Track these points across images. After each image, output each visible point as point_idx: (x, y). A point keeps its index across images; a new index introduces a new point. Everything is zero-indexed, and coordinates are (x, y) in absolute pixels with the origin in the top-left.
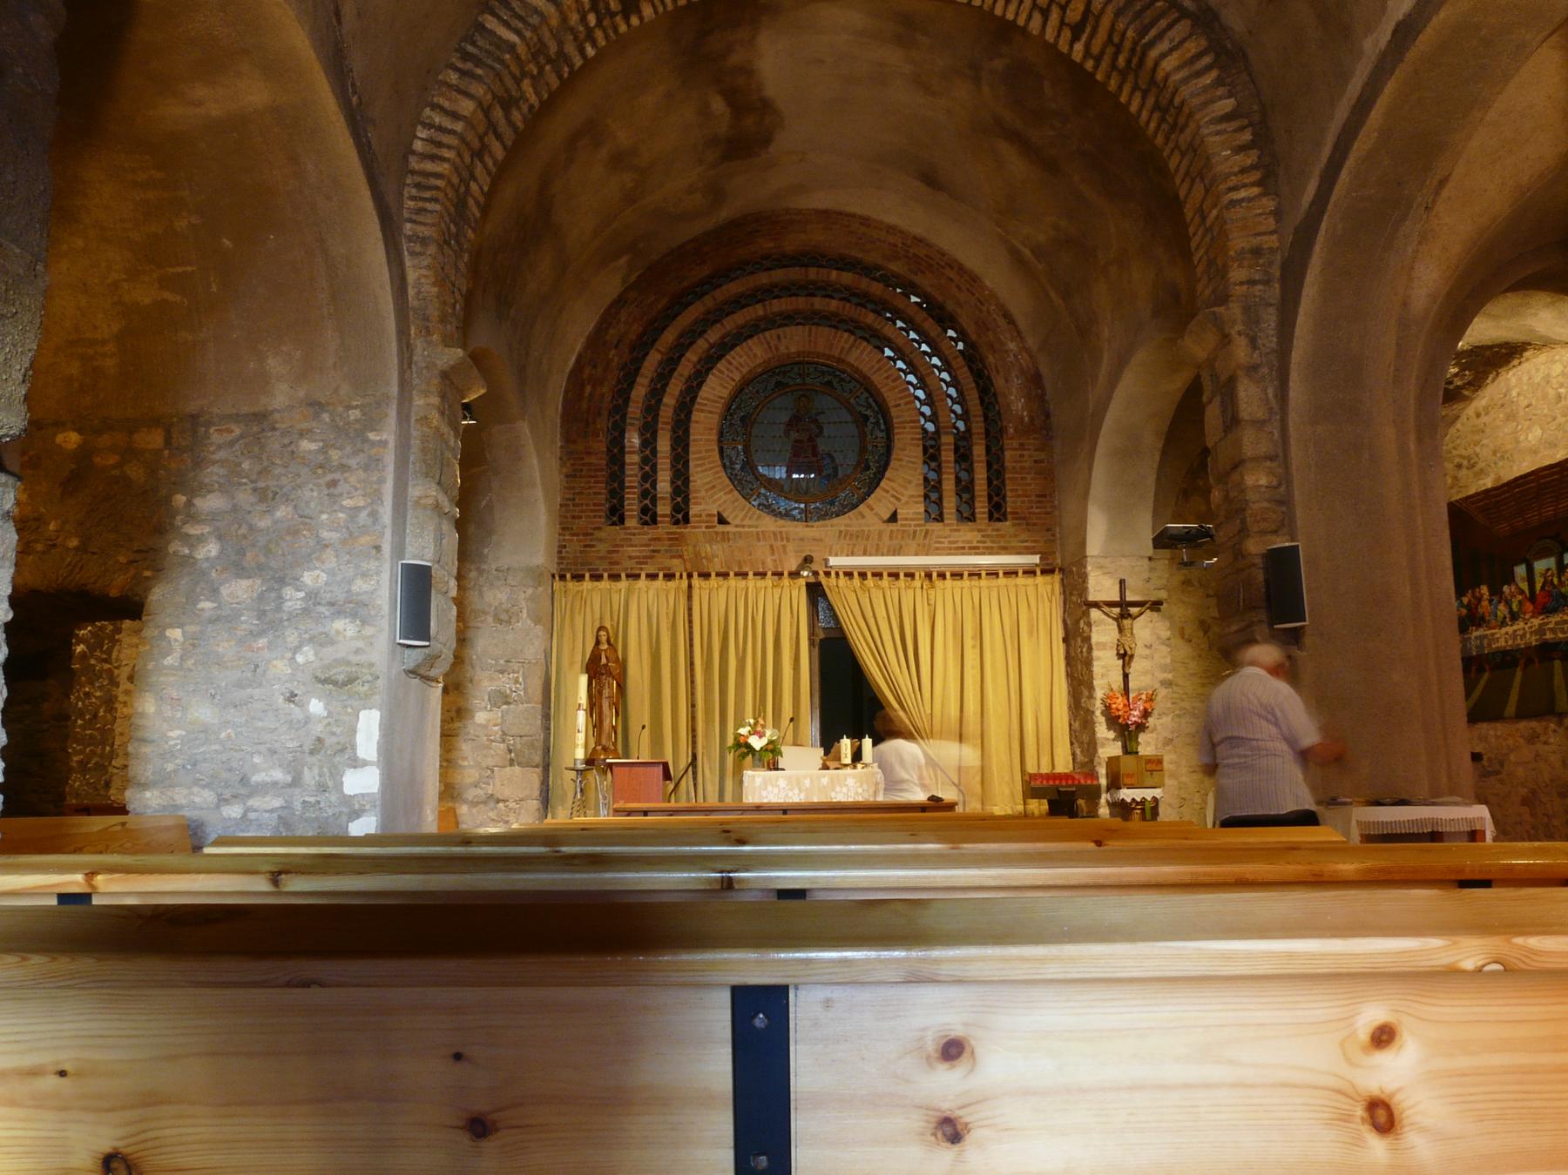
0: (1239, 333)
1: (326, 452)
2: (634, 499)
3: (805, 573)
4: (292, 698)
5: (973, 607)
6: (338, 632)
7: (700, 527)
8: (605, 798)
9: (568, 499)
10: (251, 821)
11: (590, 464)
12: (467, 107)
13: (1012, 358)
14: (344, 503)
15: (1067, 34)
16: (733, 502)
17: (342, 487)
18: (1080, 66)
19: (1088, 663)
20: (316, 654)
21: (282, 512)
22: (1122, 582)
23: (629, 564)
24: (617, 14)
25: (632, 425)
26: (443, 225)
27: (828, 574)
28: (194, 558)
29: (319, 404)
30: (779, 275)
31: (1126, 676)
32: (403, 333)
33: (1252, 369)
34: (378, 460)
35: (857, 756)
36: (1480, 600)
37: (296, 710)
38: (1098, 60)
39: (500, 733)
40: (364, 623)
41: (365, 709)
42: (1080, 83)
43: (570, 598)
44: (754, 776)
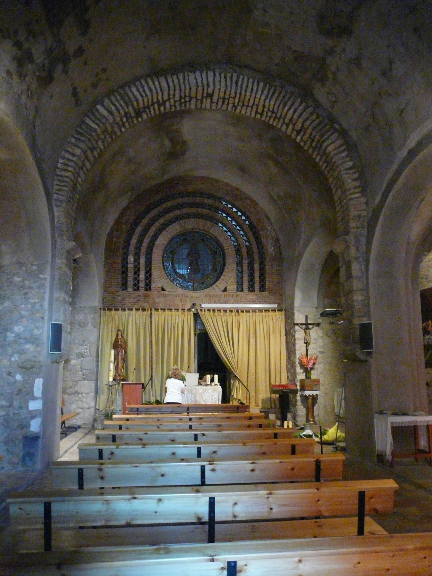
0: (353, 246)
1: (24, 282)
3: (193, 310)
4: (9, 374)
5: (253, 323)
6: (27, 349)
8: (119, 393)
9: (107, 280)
12: (78, 152)
13: (269, 233)
14: (30, 301)
15: (295, 133)
17: (30, 295)
18: (299, 144)
19: (294, 345)
20: (19, 357)
21: (7, 304)
22: (306, 317)
24: (134, 118)
25: (131, 253)
27: (201, 310)
29: (21, 263)
30: (186, 200)
31: (307, 350)
32: (53, 236)
33: (357, 258)
35: (212, 380)
36: (428, 325)
38: (305, 143)
40: (37, 346)
41: (37, 378)
42: (298, 147)
43: (107, 318)
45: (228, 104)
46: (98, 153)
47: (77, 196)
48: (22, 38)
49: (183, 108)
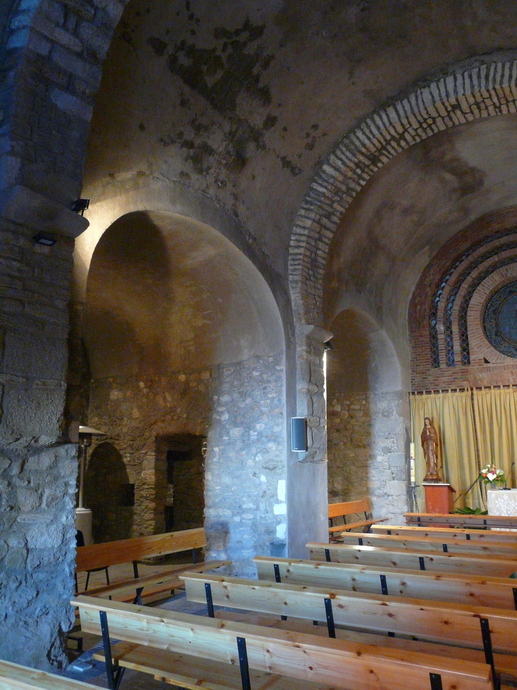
1: (262, 376)
2: (443, 355)
4: (255, 474)
6: (270, 448)
7: (476, 365)
9: (414, 358)
10: (243, 523)
11: (423, 341)
14: (269, 396)
16: (491, 353)
17: (268, 390)
21: (248, 401)
23: (443, 385)
25: (440, 321)
26: (304, 274)
28: (221, 420)
29: (259, 356)
30: (504, 240)
34: (280, 377)
37: (257, 480)
39: (388, 465)
40: (279, 444)
43: (417, 403)
44: (491, 493)
45: (487, 108)
46: (338, 217)
47: (321, 271)
48: (189, 135)
49: (430, 133)
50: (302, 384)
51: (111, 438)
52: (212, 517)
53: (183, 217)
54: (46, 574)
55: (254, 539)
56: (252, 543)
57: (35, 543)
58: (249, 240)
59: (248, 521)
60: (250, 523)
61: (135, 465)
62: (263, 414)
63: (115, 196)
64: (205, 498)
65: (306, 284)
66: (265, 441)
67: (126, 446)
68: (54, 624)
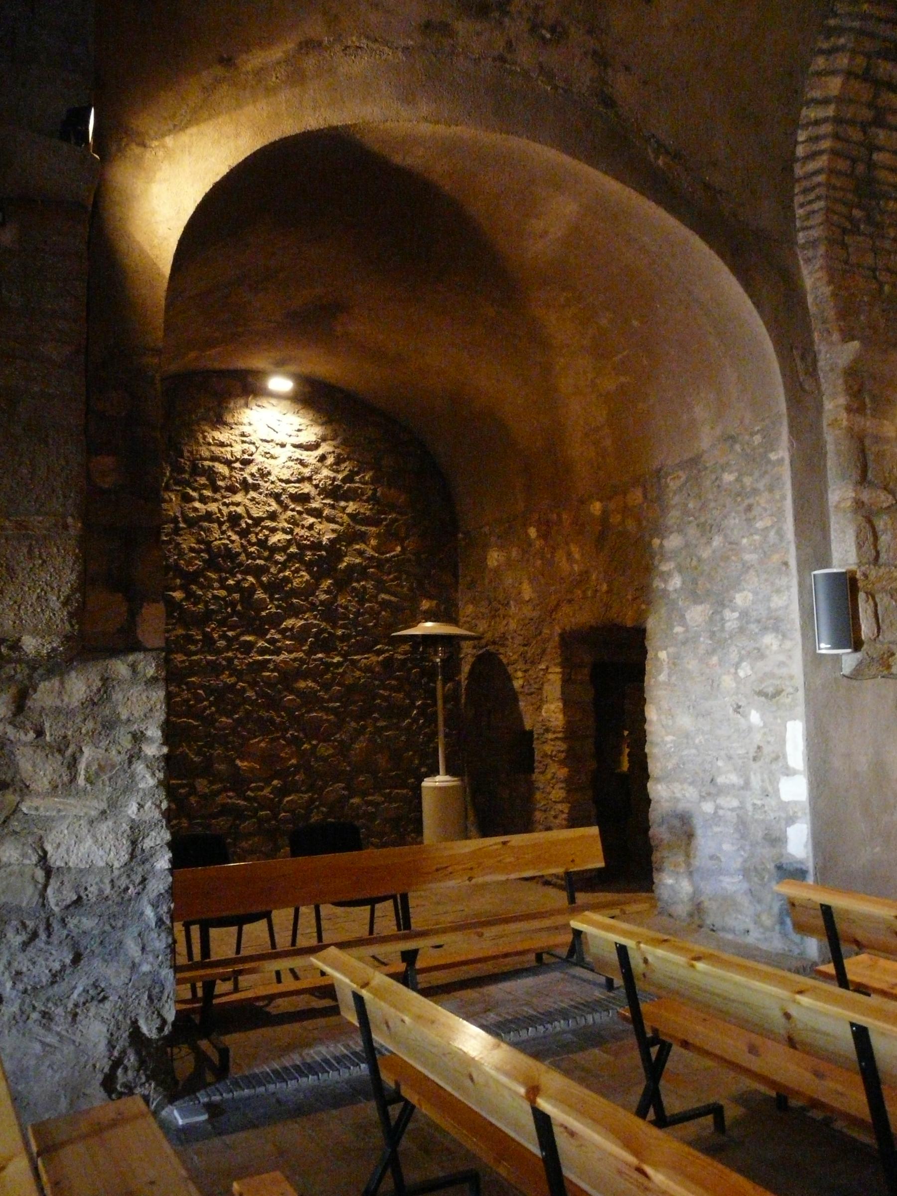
1: (742, 481)
4: (738, 708)
10: (720, 817)
17: (756, 511)
21: (717, 541)
37: (742, 720)
40: (784, 636)
50: (840, 489)
51: (494, 643)
52: (663, 800)
53: (441, 129)
54: (96, 921)
55: (743, 853)
56: (737, 864)
57: (66, 856)
58: (657, 158)
59: (729, 813)
60: (732, 817)
61: (532, 694)
62: (749, 568)
63: (239, 106)
64: (649, 760)
65: (844, 246)
66: (757, 630)
67: (515, 657)
68: (117, 1022)
